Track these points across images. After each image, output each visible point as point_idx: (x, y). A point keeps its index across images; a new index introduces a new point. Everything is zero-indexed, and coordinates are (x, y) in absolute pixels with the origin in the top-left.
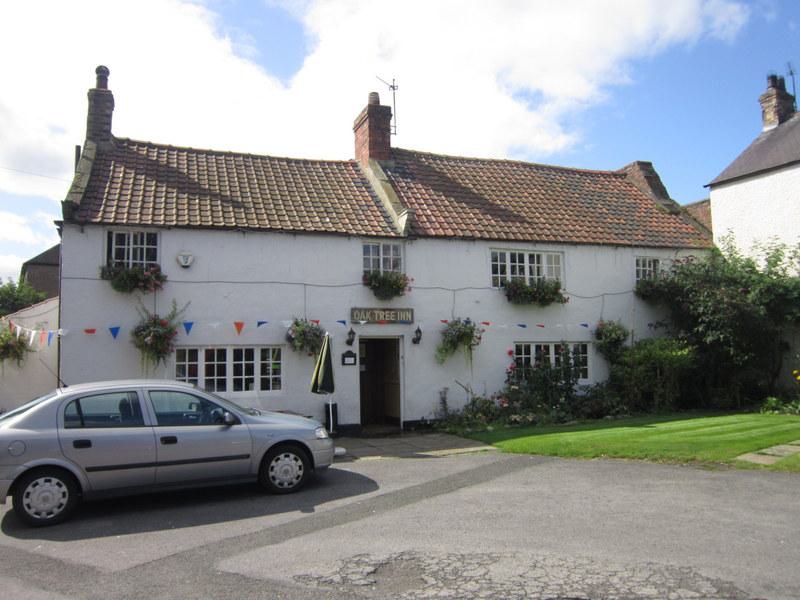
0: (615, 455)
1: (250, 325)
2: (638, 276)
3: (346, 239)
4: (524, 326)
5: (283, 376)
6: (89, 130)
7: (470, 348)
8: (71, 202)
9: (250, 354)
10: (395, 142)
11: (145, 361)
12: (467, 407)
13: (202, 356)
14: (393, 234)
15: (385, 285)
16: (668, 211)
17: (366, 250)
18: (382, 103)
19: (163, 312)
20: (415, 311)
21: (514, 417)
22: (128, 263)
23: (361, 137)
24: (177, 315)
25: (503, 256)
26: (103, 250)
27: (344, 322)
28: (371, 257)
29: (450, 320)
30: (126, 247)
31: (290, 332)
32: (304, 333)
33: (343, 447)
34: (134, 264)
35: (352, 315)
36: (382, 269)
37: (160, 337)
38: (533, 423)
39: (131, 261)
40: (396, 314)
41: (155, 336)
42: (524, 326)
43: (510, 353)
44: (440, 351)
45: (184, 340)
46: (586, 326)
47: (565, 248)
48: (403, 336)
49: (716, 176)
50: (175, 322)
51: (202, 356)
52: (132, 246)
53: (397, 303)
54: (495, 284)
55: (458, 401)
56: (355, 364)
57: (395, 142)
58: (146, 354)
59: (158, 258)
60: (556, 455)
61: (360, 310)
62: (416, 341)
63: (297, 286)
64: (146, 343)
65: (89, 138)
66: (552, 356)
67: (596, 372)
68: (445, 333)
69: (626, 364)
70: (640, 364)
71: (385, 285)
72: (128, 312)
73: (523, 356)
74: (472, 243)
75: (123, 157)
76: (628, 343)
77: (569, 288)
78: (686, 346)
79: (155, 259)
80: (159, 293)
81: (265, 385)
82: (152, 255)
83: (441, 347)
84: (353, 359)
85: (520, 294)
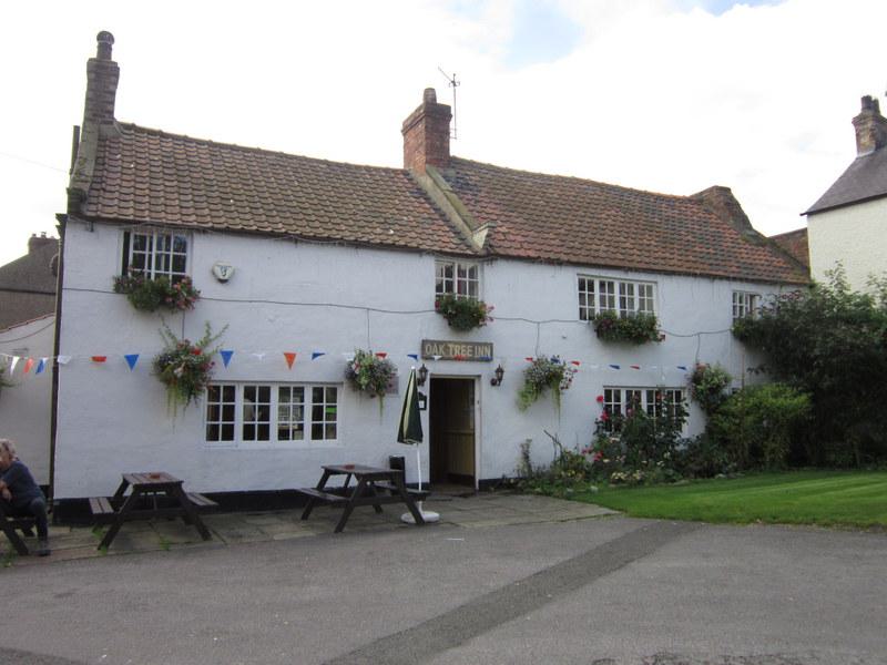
0: (774, 520)
1: (303, 356)
2: (734, 314)
4: (617, 367)
5: (339, 422)
6: (87, 110)
7: (558, 394)
8: (74, 189)
9: (299, 391)
10: (458, 149)
11: (172, 404)
12: (555, 462)
14: (469, 252)
15: (462, 313)
16: (755, 242)
18: (439, 101)
19: (195, 340)
21: (616, 475)
22: (149, 274)
23: (412, 142)
24: (210, 340)
26: (118, 253)
27: (415, 357)
29: (535, 359)
30: (147, 253)
31: (354, 366)
32: (371, 368)
33: (433, 510)
34: (157, 275)
35: (423, 349)
37: (194, 369)
38: (641, 482)
39: (153, 271)
40: (473, 349)
41: (187, 368)
42: (617, 367)
43: (599, 399)
44: (523, 395)
45: (220, 374)
46: (683, 368)
47: (659, 278)
48: (479, 376)
49: (813, 204)
50: (208, 351)
51: (240, 394)
52: (154, 252)
53: (476, 335)
54: (582, 317)
55: (544, 456)
57: (458, 149)
58: (173, 394)
59: (187, 269)
60: (700, 520)
61: (432, 342)
63: (355, 311)
64: (175, 377)
65: (86, 119)
66: (644, 404)
67: (692, 426)
68: (530, 373)
69: (734, 415)
70: (748, 414)
71: (462, 313)
72: (148, 339)
73: (613, 403)
74: (558, 268)
75: (131, 145)
76: (727, 391)
77: (663, 324)
78: (800, 393)
79: (183, 270)
80: (188, 315)
81: (317, 433)
82: (180, 264)
83: (523, 389)
85: (614, 328)
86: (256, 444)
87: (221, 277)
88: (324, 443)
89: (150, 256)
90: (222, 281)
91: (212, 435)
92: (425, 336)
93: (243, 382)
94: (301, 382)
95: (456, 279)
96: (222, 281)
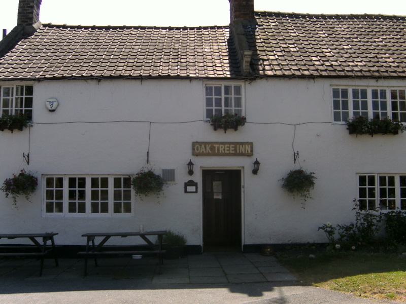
3: (312, 80)
6: (19, 19)
13: (66, 183)
17: (208, 90)
20: (255, 145)
25: (383, 94)
28: (379, 100)
36: (223, 108)
40: (235, 147)
54: (337, 117)
56: (196, 192)
62: (255, 172)
84: (194, 187)
86: (77, 215)
87: (50, 109)
88: (123, 215)
89: (12, 99)
90: (53, 111)
91: (49, 209)
92: (195, 140)
93: (113, 174)
94: (61, 175)
95: (223, 96)
96: (53, 111)
